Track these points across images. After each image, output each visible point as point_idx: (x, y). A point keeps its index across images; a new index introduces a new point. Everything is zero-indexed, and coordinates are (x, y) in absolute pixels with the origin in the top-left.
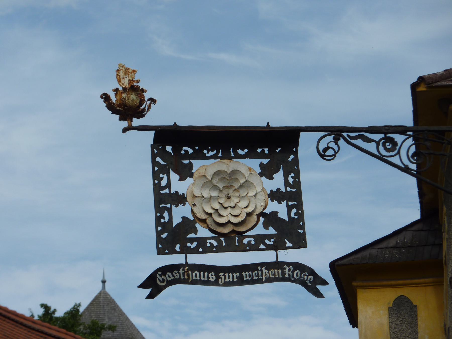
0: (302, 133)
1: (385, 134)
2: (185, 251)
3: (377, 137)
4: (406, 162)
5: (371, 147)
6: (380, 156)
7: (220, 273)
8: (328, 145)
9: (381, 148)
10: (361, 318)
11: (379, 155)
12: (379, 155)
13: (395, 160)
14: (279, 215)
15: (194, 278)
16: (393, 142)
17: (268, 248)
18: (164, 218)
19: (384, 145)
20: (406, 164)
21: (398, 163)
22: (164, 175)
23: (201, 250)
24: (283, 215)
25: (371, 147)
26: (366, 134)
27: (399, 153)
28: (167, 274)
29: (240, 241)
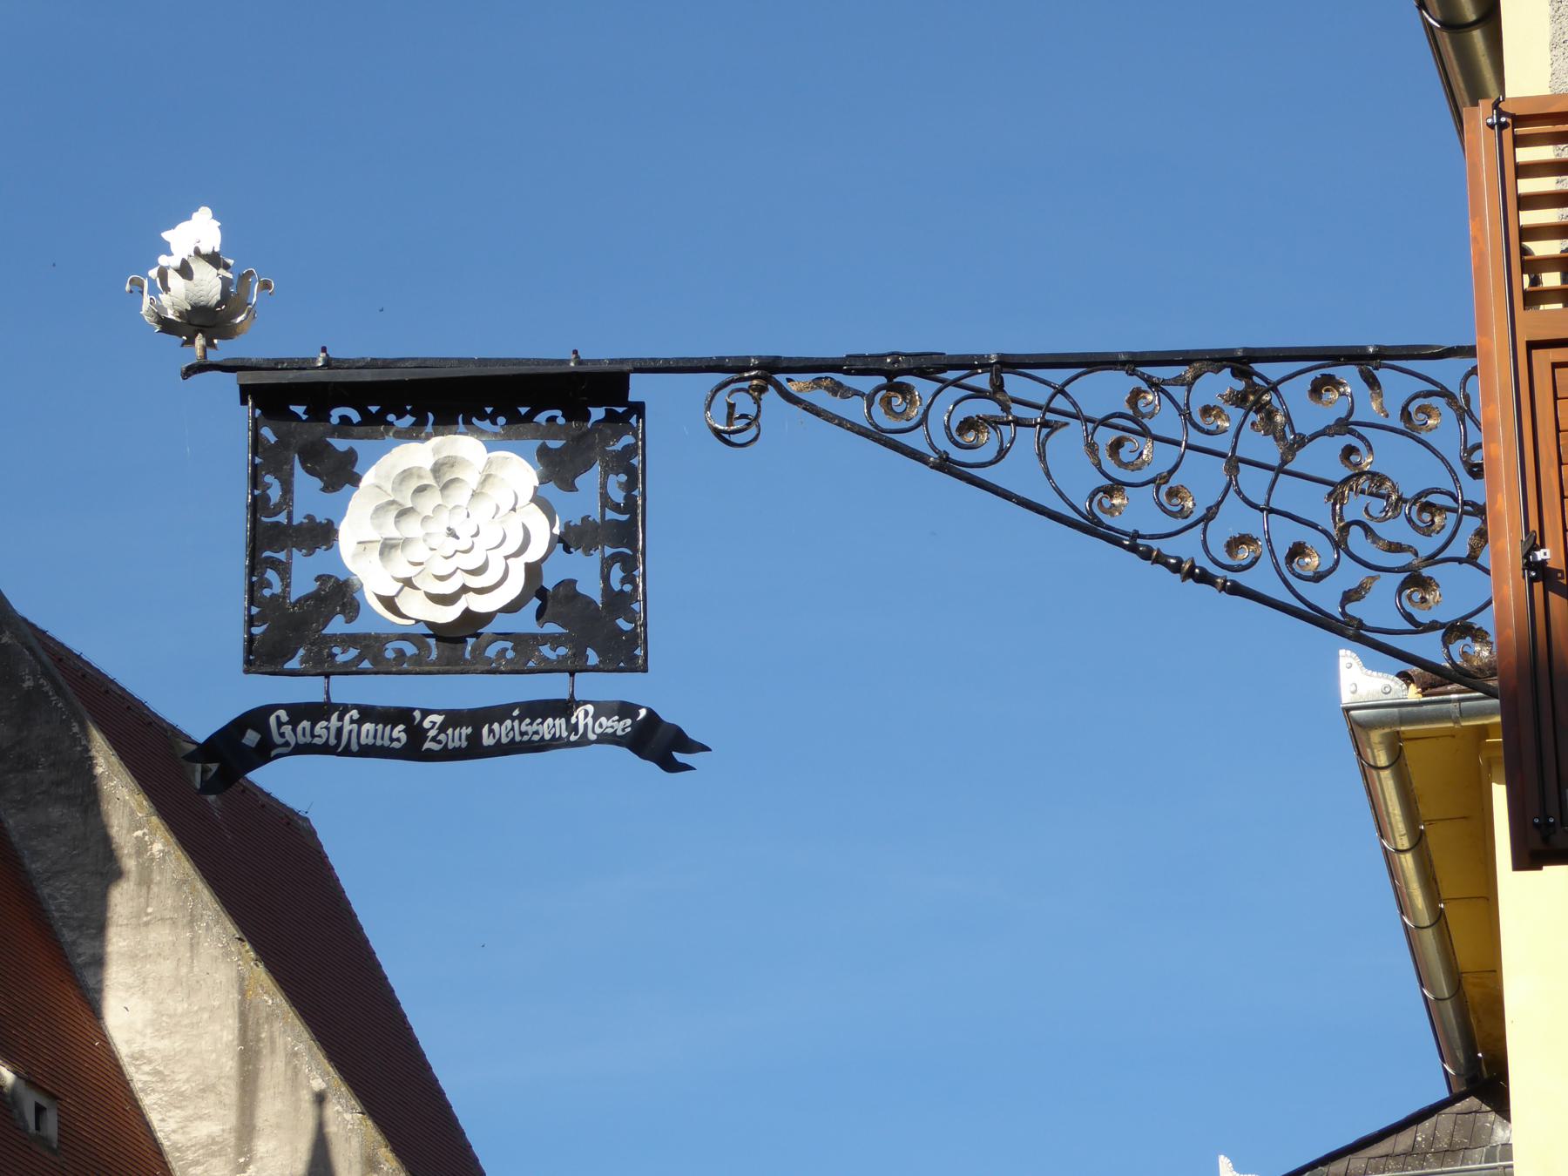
0: (631, 375)
1: (889, 374)
2: (324, 668)
3: (868, 383)
4: (944, 444)
5: (854, 410)
6: (1311, 611)
7: (440, 750)
8: (759, 427)
9: (878, 411)
10: (419, 587)
11: (871, 428)
12: (871, 428)
13: (915, 440)
14: (580, 588)
15: (363, 741)
16: (905, 390)
17: (548, 668)
18: (269, 585)
19: (887, 403)
20: (941, 448)
21: (924, 448)
22: (512, 652)
23: (366, 664)
24: (591, 588)
25: (854, 410)
26: (839, 377)
27: (924, 420)
28: (276, 714)
29: (478, 651)
